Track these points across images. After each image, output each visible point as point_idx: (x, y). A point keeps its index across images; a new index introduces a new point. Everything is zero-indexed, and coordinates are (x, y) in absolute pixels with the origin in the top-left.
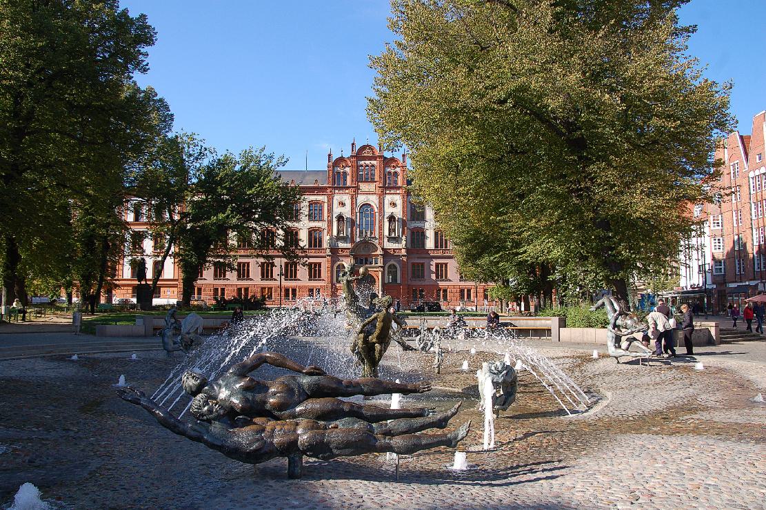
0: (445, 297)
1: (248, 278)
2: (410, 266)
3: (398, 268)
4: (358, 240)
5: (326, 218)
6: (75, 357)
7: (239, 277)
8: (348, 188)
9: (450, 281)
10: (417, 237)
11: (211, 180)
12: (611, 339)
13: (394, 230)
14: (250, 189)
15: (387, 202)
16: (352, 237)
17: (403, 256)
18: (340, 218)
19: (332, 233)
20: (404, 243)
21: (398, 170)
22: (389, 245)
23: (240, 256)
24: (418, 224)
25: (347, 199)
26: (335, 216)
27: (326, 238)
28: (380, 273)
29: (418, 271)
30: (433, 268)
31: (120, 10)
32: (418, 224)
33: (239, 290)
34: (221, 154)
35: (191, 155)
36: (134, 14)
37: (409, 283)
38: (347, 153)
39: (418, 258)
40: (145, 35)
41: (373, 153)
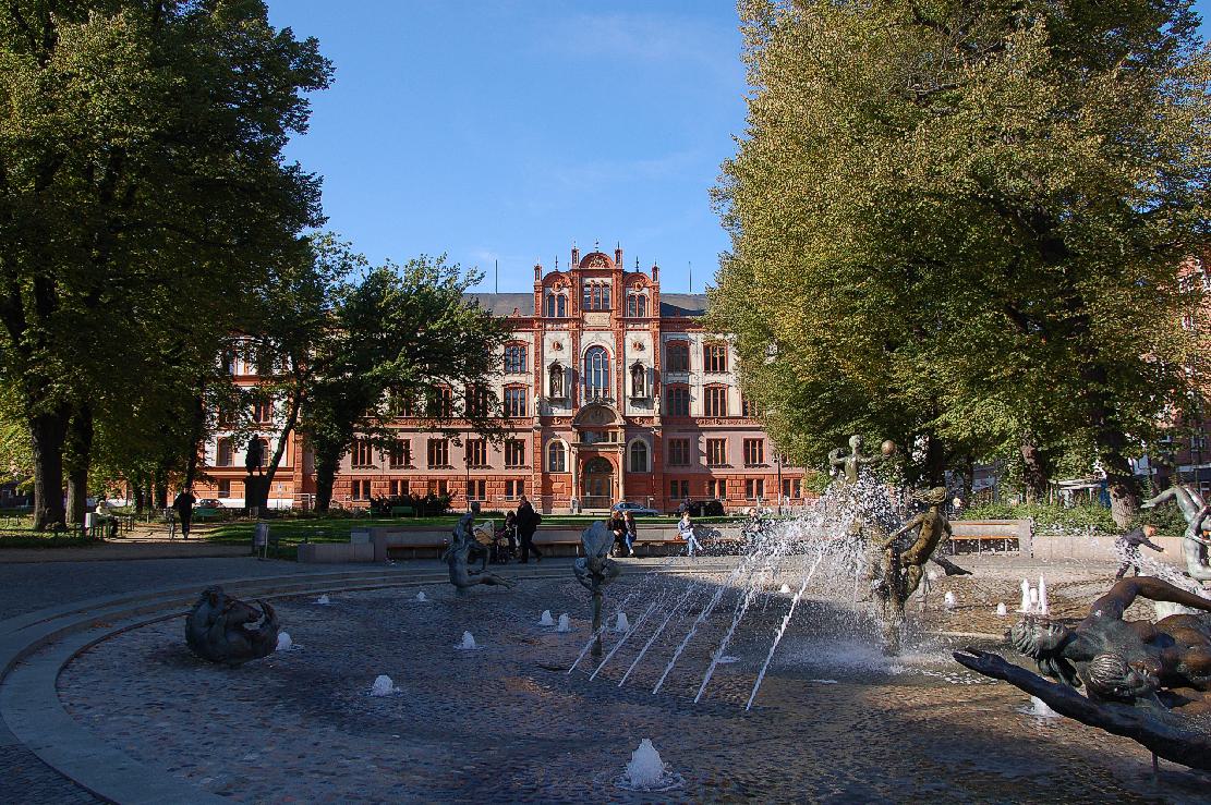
0: (722, 491)
1: (485, 466)
2: (667, 443)
3: (649, 449)
4: (583, 404)
5: (532, 368)
6: (324, 600)
7: (393, 465)
8: (647, 321)
9: (730, 466)
10: (677, 398)
11: (369, 304)
12: (1192, 552)
13: (642, 389)
14: (434, 321)
15: (629, 343)
16: (575, 397)
17: (657, 428)
18: (555, 368)
19: (543, 392)
20: (657, 406)
21: (645, 291)
22: (632, 411)
23: (402, 430)
24: (675, 378)
25: (565, 338)
26: (629, 364)
27: (533, 401)
28: (621, 456)
29: (680, 452)
30: (703, 448)
31: (278, 32)
32: (675, 378)
33: (394, 483)
34: (377, 263)
35: (327, 268)
36: (300, 37)
37: (666, 470)
38: (565, 266)
39: (679, 431)
40: (313, 71)
41: (607, 265)
